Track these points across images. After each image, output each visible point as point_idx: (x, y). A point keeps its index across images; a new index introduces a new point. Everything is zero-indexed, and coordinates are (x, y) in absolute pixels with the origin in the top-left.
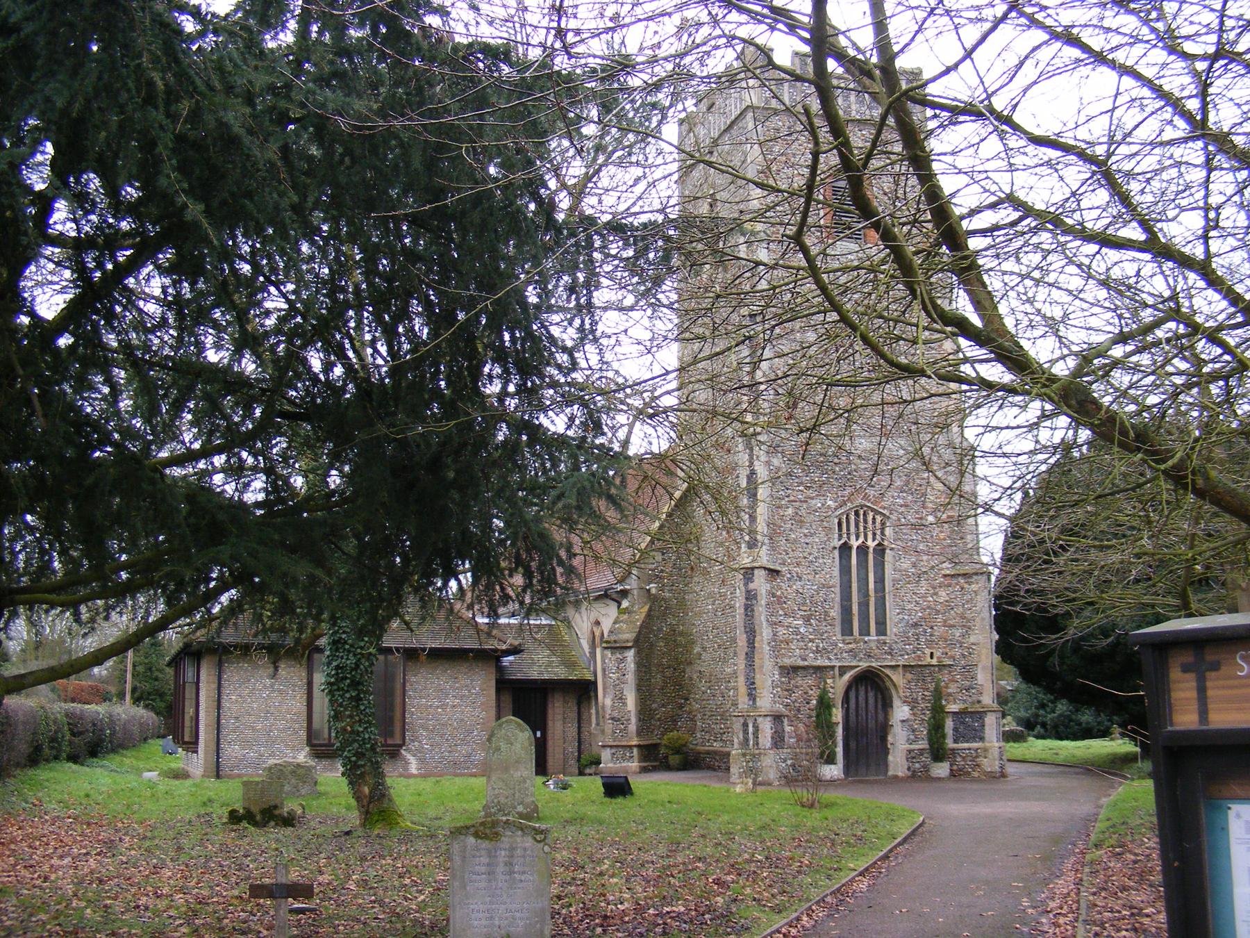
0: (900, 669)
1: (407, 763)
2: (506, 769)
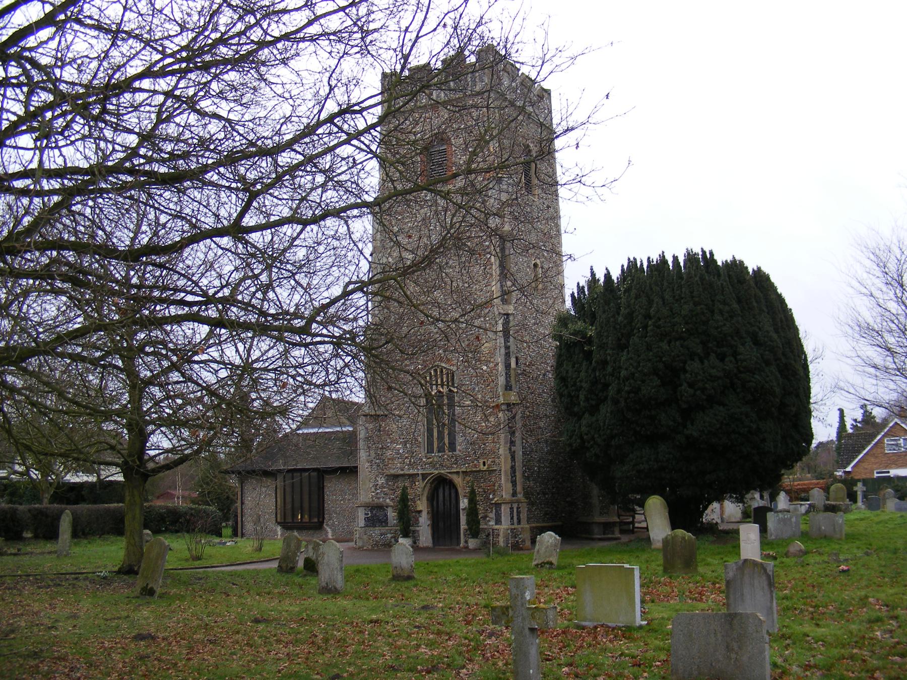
0: (461, 474)
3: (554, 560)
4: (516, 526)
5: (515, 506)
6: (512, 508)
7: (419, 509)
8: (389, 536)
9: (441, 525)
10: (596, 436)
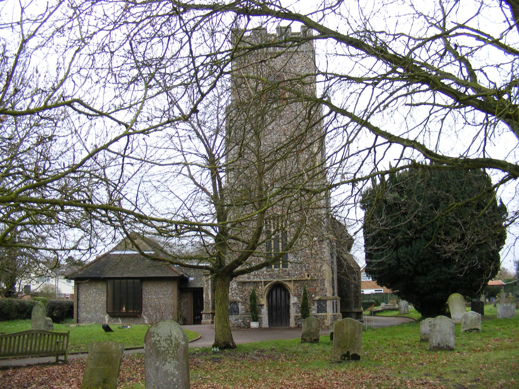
0: (292, 282)
1: (144, 319)
2: (36, 321)
3: (479, 327)
4: (335, 314)
5: (335, 301)
6: (333, 303)
7: (261, 303)
8: (240, 321)
9: (274, 313)
10: (411, 259)
